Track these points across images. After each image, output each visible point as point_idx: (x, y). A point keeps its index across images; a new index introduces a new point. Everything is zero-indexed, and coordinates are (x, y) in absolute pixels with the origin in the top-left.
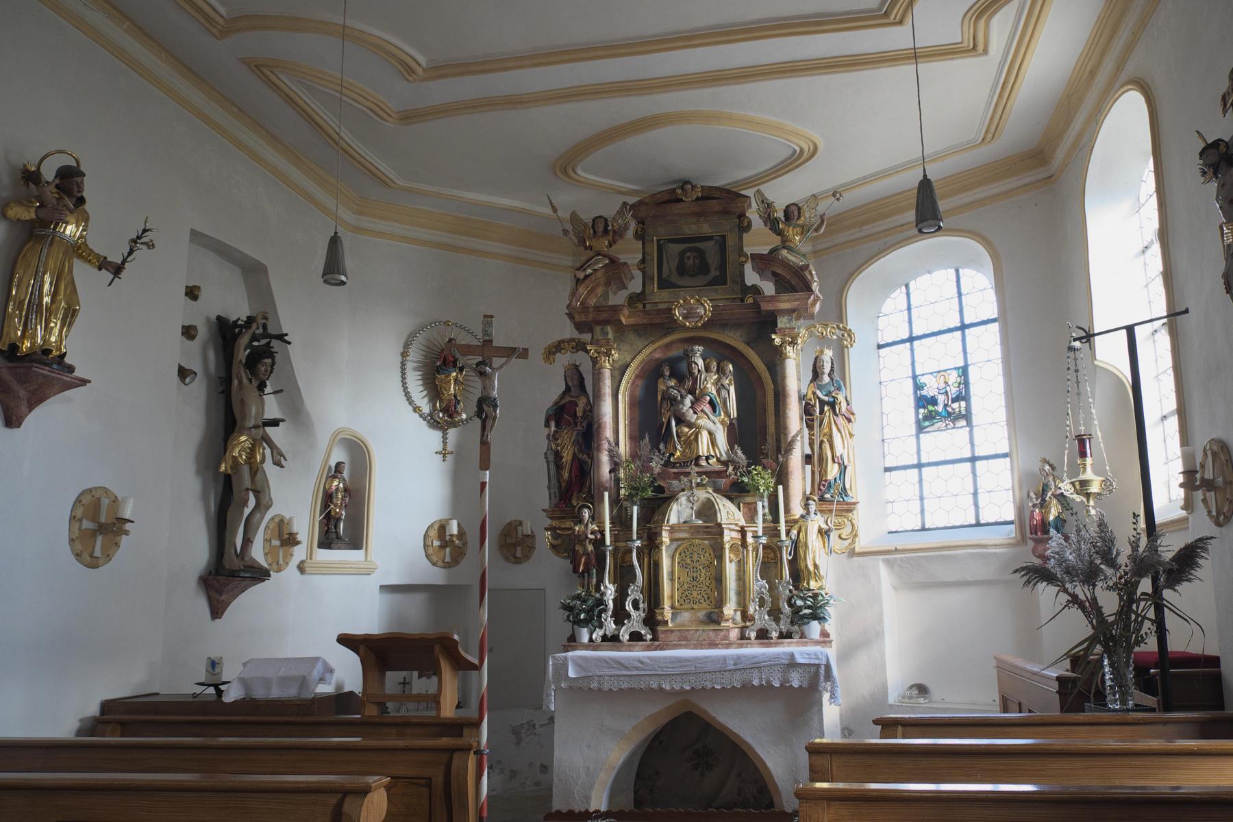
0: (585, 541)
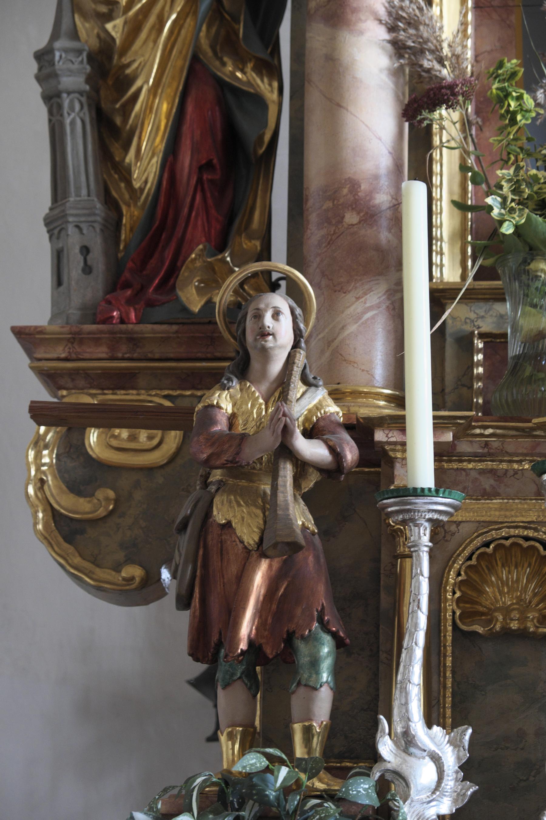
0: (275, 475)
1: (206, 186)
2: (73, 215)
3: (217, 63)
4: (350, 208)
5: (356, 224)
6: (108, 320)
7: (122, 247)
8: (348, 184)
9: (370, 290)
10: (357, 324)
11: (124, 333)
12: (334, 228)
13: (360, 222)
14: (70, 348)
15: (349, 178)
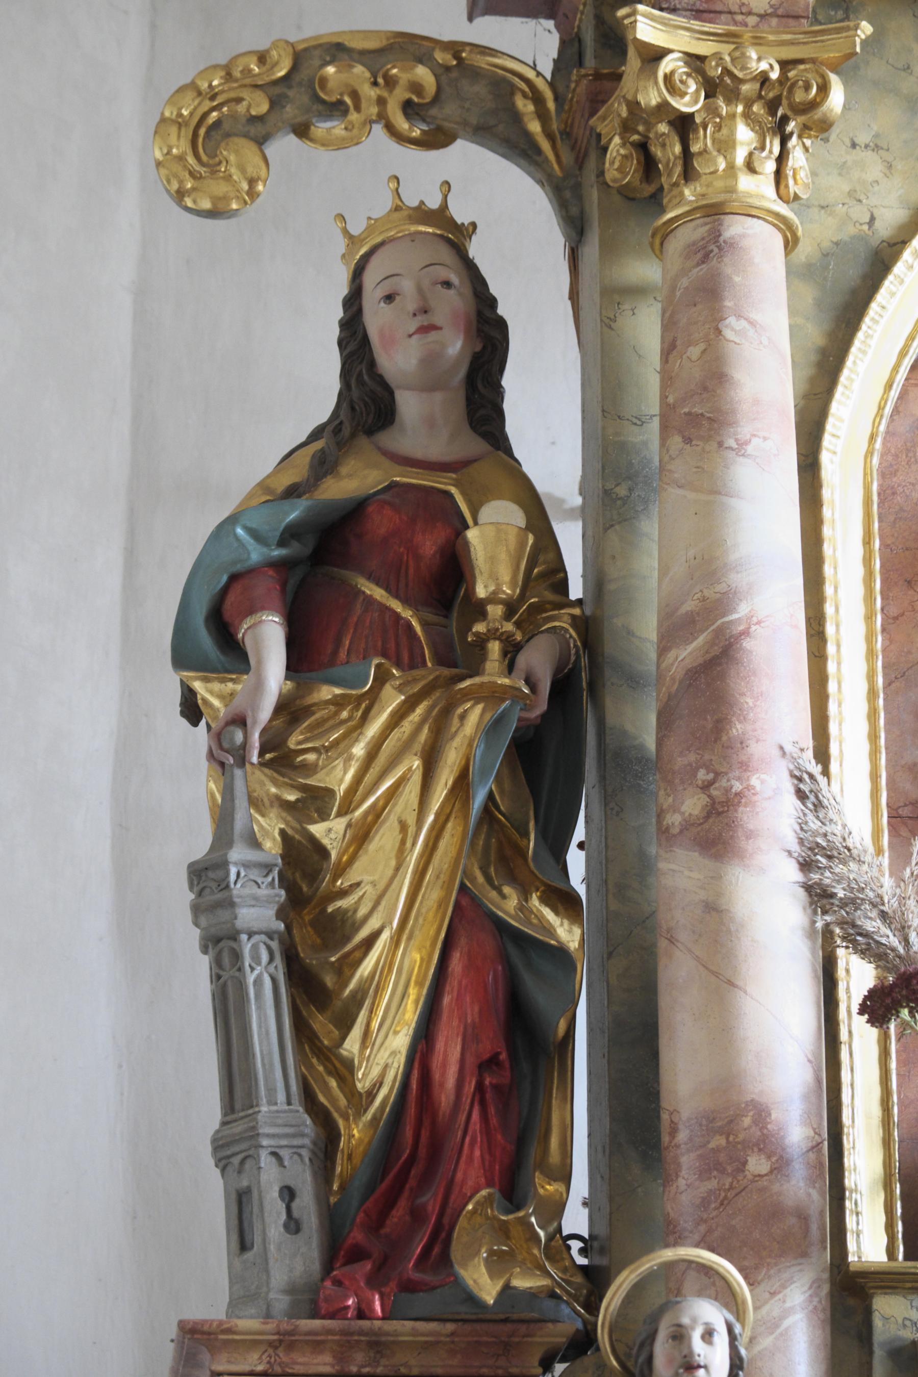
1: (489, 1096)
2: (268, 1136)
3: (494, 894)
4: (756, 1149)
5: (766, 1175)
6: (337, 1313)
7: (335, 1187)
8: (750, 1111)
9: (791, 1281)
10: (774, 1336)
11: (366, 1334)
12: (730, 1180)
13: (771, 1172)
14: (270, 1356)
15: (752, 1100)
